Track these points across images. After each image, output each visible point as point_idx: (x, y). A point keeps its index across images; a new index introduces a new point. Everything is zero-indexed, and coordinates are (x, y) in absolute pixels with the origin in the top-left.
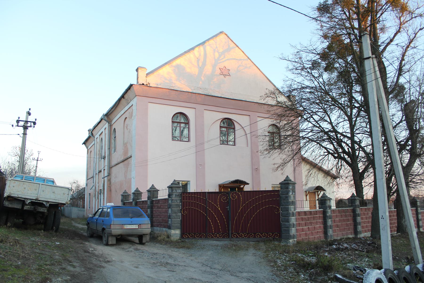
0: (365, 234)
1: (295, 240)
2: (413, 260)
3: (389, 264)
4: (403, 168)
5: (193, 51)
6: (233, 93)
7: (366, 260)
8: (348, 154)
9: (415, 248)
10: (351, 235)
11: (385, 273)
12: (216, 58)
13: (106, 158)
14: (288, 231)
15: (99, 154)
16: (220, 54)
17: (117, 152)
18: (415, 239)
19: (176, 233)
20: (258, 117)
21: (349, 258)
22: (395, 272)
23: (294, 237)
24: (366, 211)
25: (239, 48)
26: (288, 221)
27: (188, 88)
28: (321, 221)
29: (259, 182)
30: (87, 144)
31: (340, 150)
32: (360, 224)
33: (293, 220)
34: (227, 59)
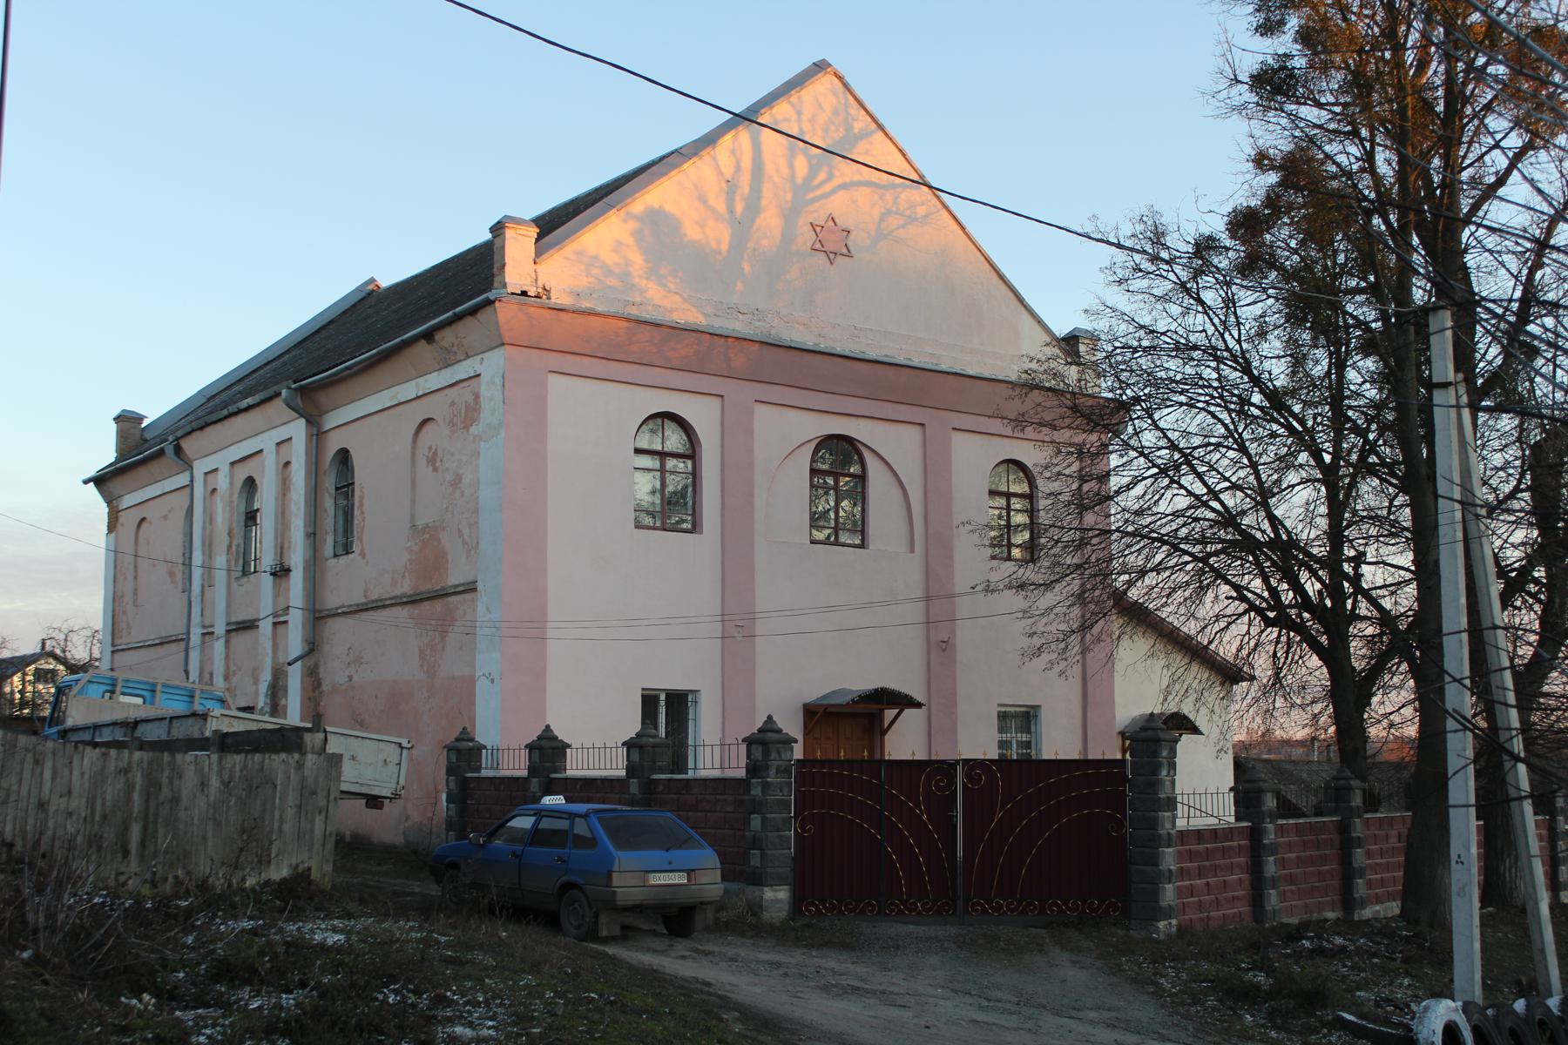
0: (1377, 908)
1: (1174, 922)
2: (1536, 988)
3: (1474, 992)
4: (1517, 675)
5: (712, 153)
6: (861, 329)
7: (1406, 982)
8: (1317, 610)
9: (1542, 951)
10: (1333, 911)
11: (1465, 1010)
12: (799, 180)
13: (297, 579)
14: (1155, 894)
15: (229, 547)
16: (814, 161)
17: (363, 555)
18: (1543, 926)
19: (777, 897)
20: (954, 429)
21: (1358, 978)
22: (1490, 1012)
23: (1168, 913)
24: (1380, 829)
25: (887, 135)
26: (1154, 860)
27: (693, 310)
28: (1242, 860)
29: (954, 694)
30: (115, 486)
31: (1288, 597)
32: (1361, 873)
33: (1169, 858)
34: (837, 181)
